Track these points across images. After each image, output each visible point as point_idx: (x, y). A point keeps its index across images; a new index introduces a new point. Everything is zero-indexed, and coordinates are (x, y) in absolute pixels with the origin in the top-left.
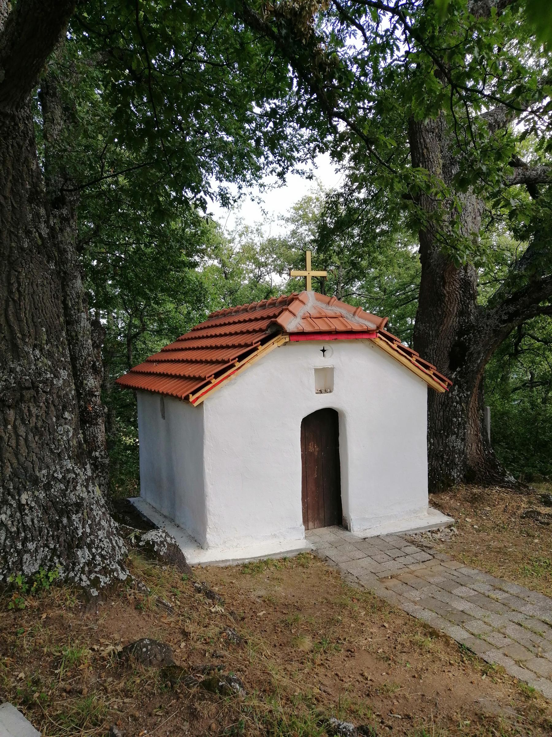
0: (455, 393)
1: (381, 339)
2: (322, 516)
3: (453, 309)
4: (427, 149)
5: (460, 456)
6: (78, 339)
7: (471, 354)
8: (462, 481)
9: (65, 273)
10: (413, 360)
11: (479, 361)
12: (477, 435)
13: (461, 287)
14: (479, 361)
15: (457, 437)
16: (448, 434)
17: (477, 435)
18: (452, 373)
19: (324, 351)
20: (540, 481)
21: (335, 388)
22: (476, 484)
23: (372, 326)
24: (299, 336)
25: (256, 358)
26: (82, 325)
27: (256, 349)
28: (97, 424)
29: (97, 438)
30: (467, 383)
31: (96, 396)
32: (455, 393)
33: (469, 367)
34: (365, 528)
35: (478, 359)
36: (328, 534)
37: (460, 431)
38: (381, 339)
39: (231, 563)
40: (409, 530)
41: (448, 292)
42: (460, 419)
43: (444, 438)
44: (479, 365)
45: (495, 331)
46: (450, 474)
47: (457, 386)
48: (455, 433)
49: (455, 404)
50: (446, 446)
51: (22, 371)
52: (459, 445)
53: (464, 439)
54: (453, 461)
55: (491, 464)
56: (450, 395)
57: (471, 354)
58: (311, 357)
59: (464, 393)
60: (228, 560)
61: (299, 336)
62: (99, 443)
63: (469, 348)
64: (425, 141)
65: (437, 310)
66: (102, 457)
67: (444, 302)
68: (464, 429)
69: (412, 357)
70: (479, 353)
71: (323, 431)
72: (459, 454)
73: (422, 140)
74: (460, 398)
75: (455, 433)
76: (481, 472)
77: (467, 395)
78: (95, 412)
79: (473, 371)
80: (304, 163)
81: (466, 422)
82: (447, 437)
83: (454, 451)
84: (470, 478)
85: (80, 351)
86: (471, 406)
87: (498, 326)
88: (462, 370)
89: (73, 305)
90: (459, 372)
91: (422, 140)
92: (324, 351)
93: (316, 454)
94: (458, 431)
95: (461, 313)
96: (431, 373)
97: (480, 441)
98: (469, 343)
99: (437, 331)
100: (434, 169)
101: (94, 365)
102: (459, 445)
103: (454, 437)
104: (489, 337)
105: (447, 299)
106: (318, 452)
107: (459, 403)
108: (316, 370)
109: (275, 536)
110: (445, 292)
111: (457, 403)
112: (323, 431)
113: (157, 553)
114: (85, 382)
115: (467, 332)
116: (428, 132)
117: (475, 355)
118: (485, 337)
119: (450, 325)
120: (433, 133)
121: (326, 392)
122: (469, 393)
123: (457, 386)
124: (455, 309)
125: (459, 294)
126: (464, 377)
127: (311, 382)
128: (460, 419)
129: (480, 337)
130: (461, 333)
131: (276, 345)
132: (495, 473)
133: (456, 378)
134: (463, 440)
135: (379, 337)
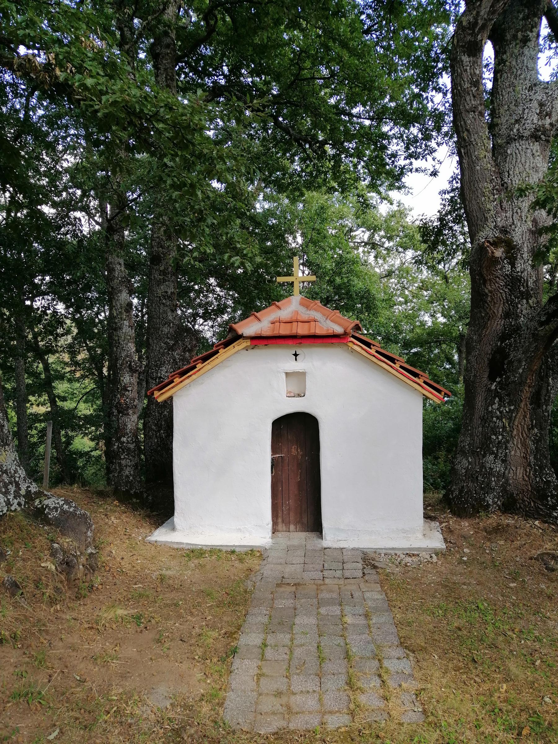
0: (496, 406)
1: (354, 344)
2: (305, 520)
3: (498, 312)
4: (468, 131)
5: (499, 480)
6: (119, 343)
7: (511, 362)
8: (499, 509)
9: (112, 288)
10: (397, 366)
11: (521, 371)
12: (525, 458)
13: (506, 285)
14: (521, 371)
15: (496, 457)
16: (485, 453)
17: (525, 458)
18: (492, 384)
19: (296, 355)
20: (529, 515)
21: (307, 393)
22: (516, 514)
23: (339, 330)
24: (259, 340)
25: (217, 361)
26: (124, 331)
27: (217, 352)
28: (128, 414)
29: (127, 426)
30: (508, 395)
31: (129, 391)
32: (496, 406)
33: (508, 377)
34: (340, 539)
35: (518, 369)
36: (299, 537)
37: (500, 451)
38: (354, 344)
39: (184, 546)
40: (382, 549)
41: (490, 292)
42: (500, 437)
43: (481, 457)
44: (521, 375)
45: (533, 334)
46: (484, 500)
47: (497, 399)
48: (493, 453)
49: (495, 419)
50: (482, 466)
51: (456, 382)
52: (499, 467)
53: (506, 461)
54: (489, 484)
55: (540, 494)
56: (490, 409)
57: (511, 362)
58: (282, 361)
59: (505, 407)
60: (183, 543)
61: (259, 340)
62: (128, 431)
63: (509, 355)
64: (465, 123)
65: (481, 312)
66: (128, 442)
67: (486, 302)
68: (506, 448)
69: (395, 363)
70: (520, 361)
71: (297, 435)
72: (498, 477)
73: (462, 123)
74: (501, 412)
75: (493, 453)
76: (524, 501)
77: (510, 409)
78: (126, 404)
79: (515, 382)
80: (424, 160)
81: (508, 442)
82: (484, 456)
83: (491, 472)
84: (509, 506)
85: (120, 353)
86: (516, 423)
87: (536, 329)
88: (501, 380)
89: (117, 314)
90: (499, 383)
91: (462, 123)
92: (296, 355)
93: (300, 457)
94: (497, 451)
95: (507, 315)
96: (420, 381)
97: (529, 465)
98: (509, 349)
99: (480, 335)
100: (476, 153)
101: (130, 365)
102: (499, 467)
103: (492, 457)
104: (529, 342)
105: (489, 299)
106: (302, 455)
107: (500, 418)
108: (287, 374)
109: (239, 530)
110: (486, 291)
111: (498, 418)
112: (297, 435)
113: (46, 516)
114: (122, 378)
115: (509, 337)
116: (468, 112)
117: (516, 364)
118: (524, 342)
119: (494, 328)
120: (474, 112)
121: (299, 396)
122: (512, 408)
123: (497, 399)
124: (500, 310)
125: (504, 293)
126: (505, 389)
127: (281, 385)
128: (500, 437)
129: (520, 343)
130: (503, 337)
131: (237, 348)
132: (542, 505)
133: (496, 389)
134: (504, 461)
135: (352, 342)
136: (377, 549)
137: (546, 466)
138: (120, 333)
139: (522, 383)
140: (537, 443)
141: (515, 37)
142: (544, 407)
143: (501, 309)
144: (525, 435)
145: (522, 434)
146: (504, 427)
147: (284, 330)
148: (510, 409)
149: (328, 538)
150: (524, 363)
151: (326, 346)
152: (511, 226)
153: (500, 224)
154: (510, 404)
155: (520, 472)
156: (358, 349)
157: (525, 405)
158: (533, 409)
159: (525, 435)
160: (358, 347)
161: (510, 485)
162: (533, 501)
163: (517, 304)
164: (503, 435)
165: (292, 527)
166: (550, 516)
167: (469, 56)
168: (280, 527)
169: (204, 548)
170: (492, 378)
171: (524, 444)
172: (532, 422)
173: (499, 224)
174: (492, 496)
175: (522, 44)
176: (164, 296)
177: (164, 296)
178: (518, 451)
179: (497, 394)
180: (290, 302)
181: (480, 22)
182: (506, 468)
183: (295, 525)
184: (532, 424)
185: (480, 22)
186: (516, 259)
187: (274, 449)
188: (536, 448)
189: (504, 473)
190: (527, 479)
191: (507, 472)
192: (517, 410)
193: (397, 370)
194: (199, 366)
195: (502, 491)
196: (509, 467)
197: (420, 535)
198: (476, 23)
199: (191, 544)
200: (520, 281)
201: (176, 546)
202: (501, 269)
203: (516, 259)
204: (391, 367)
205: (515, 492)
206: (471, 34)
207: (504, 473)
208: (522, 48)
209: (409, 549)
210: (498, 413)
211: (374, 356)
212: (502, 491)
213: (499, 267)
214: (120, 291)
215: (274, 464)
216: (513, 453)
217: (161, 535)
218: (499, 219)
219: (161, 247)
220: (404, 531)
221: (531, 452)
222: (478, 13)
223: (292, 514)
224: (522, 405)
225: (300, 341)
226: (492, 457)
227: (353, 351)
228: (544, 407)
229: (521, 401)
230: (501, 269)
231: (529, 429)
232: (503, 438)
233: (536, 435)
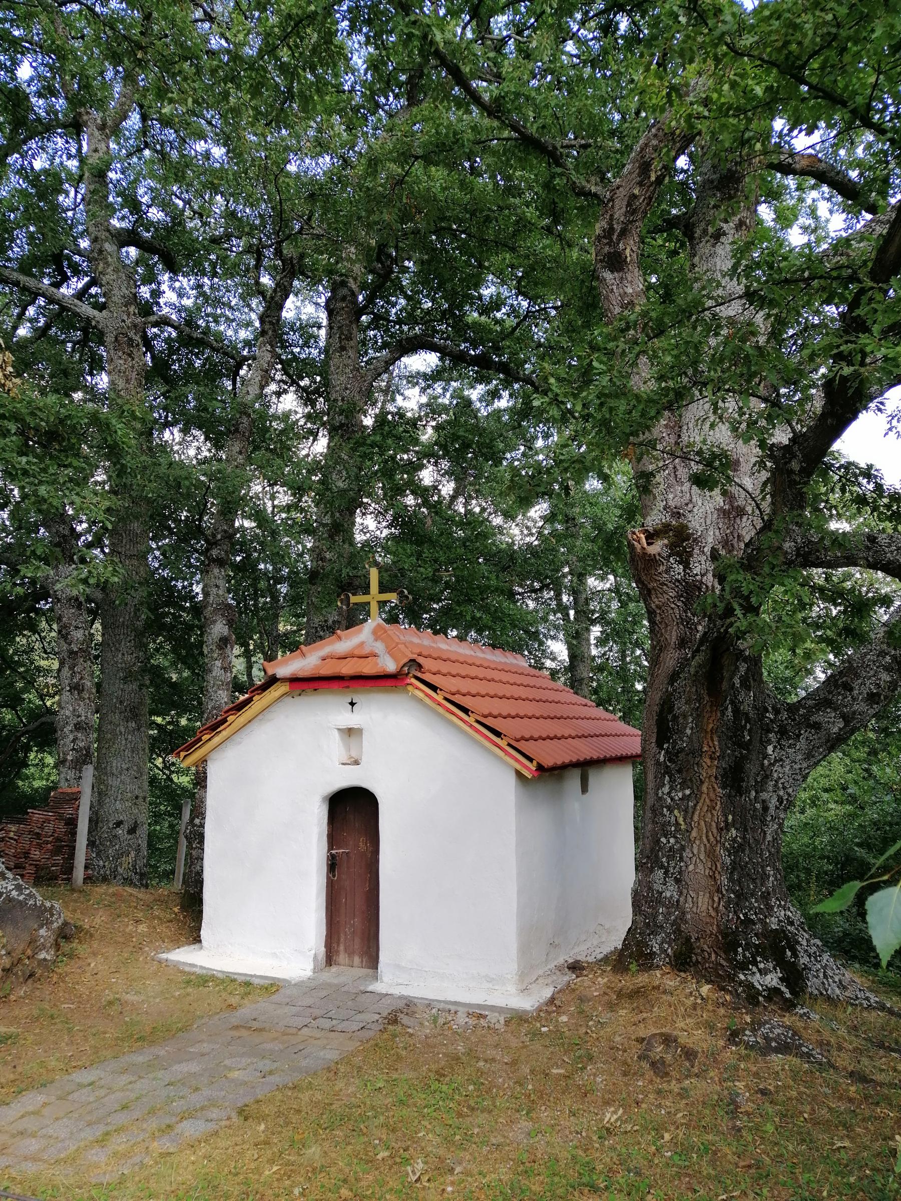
0: (666, 789)
7: (675, 718)
13: (679, 597)
15: (666, 873)
19: (352, 704)
24: (303, 684)
26: (214, 674)
30: (679, 771)
32: (666, 789)
33: (675, 742)
34: (400, 981)
37: (672, 864)
47: (667, 778)
48: (662, 867)
52: (670, 891)
58: (330, 714)
77: (684, 795)
81: (683, 848)
86: (696, 818)
92: (352, 704)
97: (719, 891)
102: (670, 891)
117: (681, 720)
122: (688, 792)
128: (672, 840)
134: (678, 881)
136: (433, 1000)
137: (752, 895)
138: (209, 677)
139: (696, 753)
140: (736, 853)
141: (705, 232)
142: (753, 793)
143: (674, 633)
144: (712, 839)
145: (707, 837)
146: (677, 824)
147: (347, 668)
148: (684, 795)
149: (385, 979)
150: (690, 720)
151: (387, 691)
152: (687, 504)
153: (672, 504)
154: (684, 785)
155: (703, 902)
156: (420, 695)
157: (712, 791)
158: (729, 796)
159: (712, 839)
160: (420, 692)
161: (687, 922)
162: (715, 952)
163: (696, 625)
164: (676, 837)
165: (357, 960)
166: (732, 978)
167: (612, 272)
168: (342, 957)
169: (256, 981)
170: (660, 746)
171: (711, 854)
172: (727, 818)
173: (671, 503)
174: (659, 938)
175: (712, 240)
176: (322, 627)
177: (322, 627)
178: (700, 866)
179: (667, 771)
180: (361, 631)
181: (618, 228)
182: (681, 893)
183: (361, 956)
184: (726, 821)
185: (618, 228)
186: (690, 554)
187: (333, 839)
188: (733, 862)
189: (678, 901)
190: (713, 914)
191: (682, 899)
192: (696, 795)
193: (471, 726)
194: (231, 719)
195: (674, 932)
196: (685, 891)
197: (512, 988)
198: (612, 229)
199: (204, 968)
200: (700, 589)
201: (187, 969)
202: (667, 571)
203: (692, 556)
204: (461, 719)
205: (694, 936)
206: (609, 244)
207: (678, 901)
208: (714, 246)
209: (479, 1006)
210: (669, 800)
211: (439, 704)
212: (674, 932)
213: (662, 568)
214: (215, 622)
215: (333, 864)
216: (691, 868)
217: (185, 956)
218: (671, 496)
219: (321, 559)
220: (490, 980)
221: (722, 868)
222: (611, 215)
223: (357, 941)
224: (704, 788)
225: (347, 684)
226: (660, 873)
227: (414, 697)
228: (753, 793)
229: (702, 782)
230: (667, 571)
231: (720, 830)
232: (677, 842)
233: (734, 840)
